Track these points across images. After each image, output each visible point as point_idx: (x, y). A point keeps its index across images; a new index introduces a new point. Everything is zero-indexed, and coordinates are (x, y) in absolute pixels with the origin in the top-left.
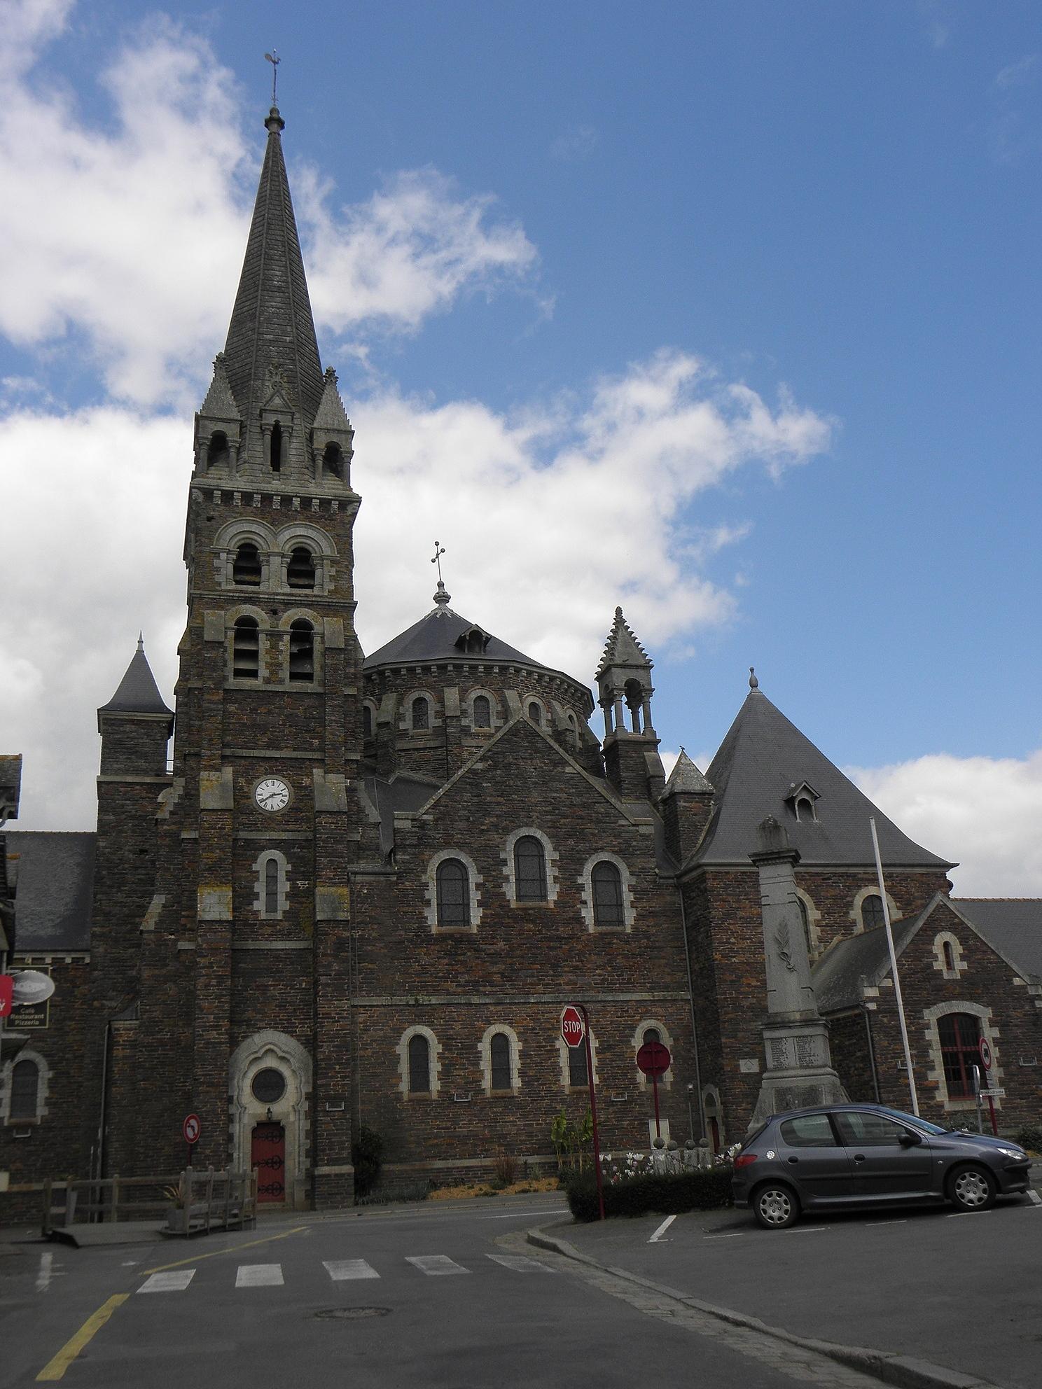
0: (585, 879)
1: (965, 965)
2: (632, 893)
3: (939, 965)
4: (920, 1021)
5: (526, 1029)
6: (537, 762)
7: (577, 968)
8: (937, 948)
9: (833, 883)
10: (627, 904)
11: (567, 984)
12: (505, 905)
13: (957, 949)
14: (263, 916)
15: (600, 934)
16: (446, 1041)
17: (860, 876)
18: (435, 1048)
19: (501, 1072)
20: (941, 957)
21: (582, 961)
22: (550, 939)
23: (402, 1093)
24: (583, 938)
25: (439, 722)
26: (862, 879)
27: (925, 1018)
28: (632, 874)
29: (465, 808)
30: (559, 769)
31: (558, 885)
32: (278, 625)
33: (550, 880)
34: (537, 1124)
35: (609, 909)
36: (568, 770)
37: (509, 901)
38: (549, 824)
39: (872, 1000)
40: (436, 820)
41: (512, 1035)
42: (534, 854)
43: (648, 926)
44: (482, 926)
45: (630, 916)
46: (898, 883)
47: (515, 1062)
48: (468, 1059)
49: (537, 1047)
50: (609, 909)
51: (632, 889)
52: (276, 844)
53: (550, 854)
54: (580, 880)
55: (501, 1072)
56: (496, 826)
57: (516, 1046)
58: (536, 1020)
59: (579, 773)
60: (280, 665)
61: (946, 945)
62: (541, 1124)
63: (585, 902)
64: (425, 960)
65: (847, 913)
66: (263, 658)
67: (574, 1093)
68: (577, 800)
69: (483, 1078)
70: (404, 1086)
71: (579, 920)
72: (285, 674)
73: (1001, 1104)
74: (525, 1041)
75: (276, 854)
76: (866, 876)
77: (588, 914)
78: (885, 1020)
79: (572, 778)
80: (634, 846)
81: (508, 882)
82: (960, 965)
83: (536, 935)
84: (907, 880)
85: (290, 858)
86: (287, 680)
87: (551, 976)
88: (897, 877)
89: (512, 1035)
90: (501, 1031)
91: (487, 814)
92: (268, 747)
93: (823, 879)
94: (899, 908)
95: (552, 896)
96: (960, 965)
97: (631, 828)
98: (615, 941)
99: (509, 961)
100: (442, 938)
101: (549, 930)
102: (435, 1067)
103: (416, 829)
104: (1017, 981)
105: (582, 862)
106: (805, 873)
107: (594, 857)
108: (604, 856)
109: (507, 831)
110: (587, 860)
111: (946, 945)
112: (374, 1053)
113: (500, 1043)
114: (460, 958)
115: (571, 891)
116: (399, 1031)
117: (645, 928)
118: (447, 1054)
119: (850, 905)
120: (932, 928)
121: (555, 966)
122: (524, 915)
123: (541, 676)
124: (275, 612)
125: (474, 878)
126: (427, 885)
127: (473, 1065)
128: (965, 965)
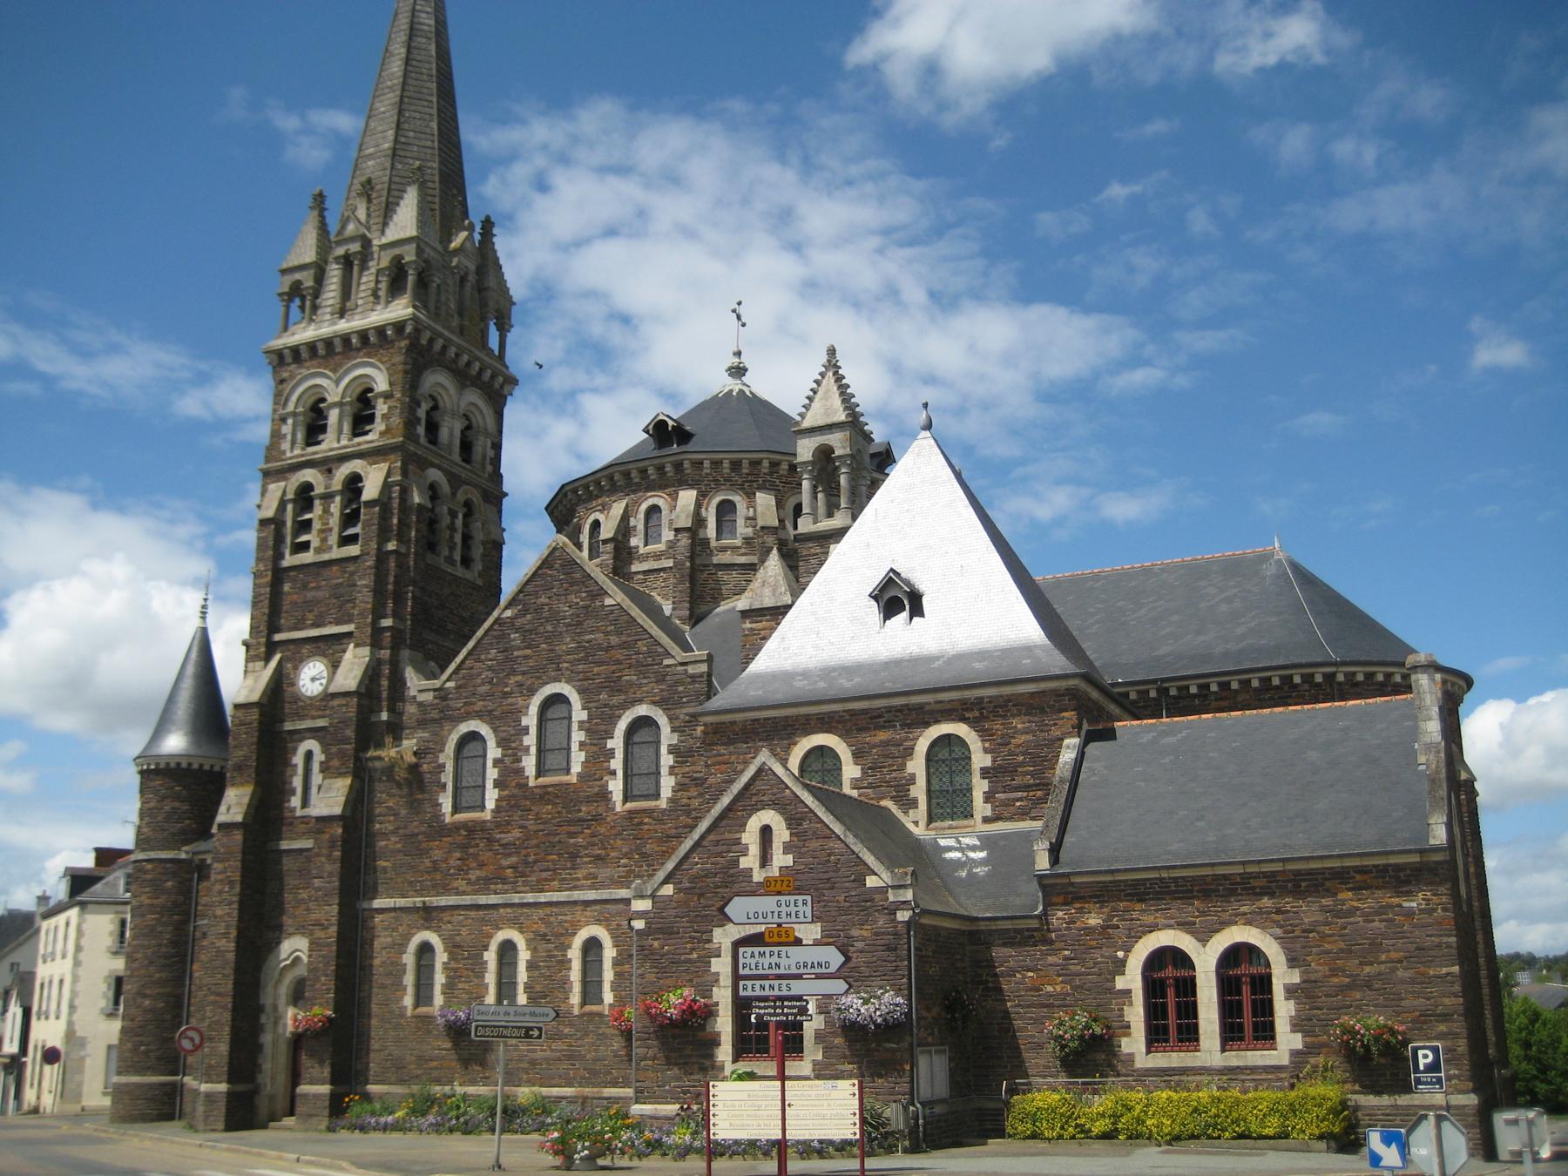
0: (616, 743)
1: (788, 860)
2: (671, 756)
3: (750, 861)
4: (707, 946)
5: (536, 933)
6: (572, 598)
7: (598, 858)
8: (750, 836)
9: (885, 722)
10: (664, 771)
11: (586, 878)
12: (523, 786)
13: (781, 834)
14: (299, 813)
15: (630, 812)
16: (453, 947)
17: (927, 708)
18: (441, 957)
19: (506, 987)
20: (754, 850)
21: (605, 849)
22: (571, 822)
23: (406, 1007)
24: (608, 819)
25: (749, 531)
26: (932, 712)
27: (715, 941)
28: (673, 730)
29: (490, 668)
30: (598, 603)
31: (583, 753)
32: (331, 484)
33: (575, 747)
34: (542, 1051)
35: (639, 780)
36: (608, 601)
37: (528, 777)
38: (581, 676)
39: (641, 915)
40: (458, 687)
41: (521, 943)
42: (562, 716)
43: (689, 798)
44: (497, 810)
45: (667, 784)
46: (991, 712)
47: (522, 976)
48: (473, 971)
49: (548, 956)
50: (639, 780)
51: (673, 750)
52: (314, 733)
53: (579, 714)
54: (610, 744)
55: (506, 987)
56: (520, 685)
57: (524, 956)
58: (548, 924)
59: (619, 604)
60: (331, 530)
61: (766, 831)
62: (545, 1051)
63: (614, 773)
64: (437, 854)
65: (903, 767)
66: (316, 525)
67: (583, 1015)
68: (614, 640)
69: (487, 993)
70: (408, 1001)
71: (605, 795)
72: (333, 539)
73: (814, 1070)
74: (534, 950)
75: (311, 744)
76: (939, 707)
77: (616, 786)
78: (656, 944)
79: (612, 612)
80: (682, 692)
81: (529, 755)
82: (781, 859)
83: (553, 818)
84: (1007, 706)
85: (325, 749)
86: (335, 547)
87: (568, 869)
88: (990, 702)
89: (521, 943)
90: (509, 937)
91: (513, 672)
92: (316, 625)
93: (871, 718)
94: (986, 751)
95: (576, 768)
96: (781, 859)
97: (679, 668)
98: (646, 820)
99: (524, 852)
100: (457, 827)
101: (569, 812)
102: (440, 978)
103: (437, 701)
104: (871, 882)
105: (613, 720)
106: (843, 711)
107: (627, 713)
108: (642, 710)
109: (532, 692)
110: (620, 717)
111: (766, 831)
112: (383, 963)
113: (508, 949)
114: (471, 850)
115: (598, 756)
116: (407, 938)
117: (685, 801)
118: (453, 965)
119: (909, 752)
120: (747, 802)
121: (574, 856)
122: (544, 794)
123: (586, 487)
124: (330, 471)
125: (493, 752)
126: (443, 766)
127: (478, 977)
128: (788, 860)
